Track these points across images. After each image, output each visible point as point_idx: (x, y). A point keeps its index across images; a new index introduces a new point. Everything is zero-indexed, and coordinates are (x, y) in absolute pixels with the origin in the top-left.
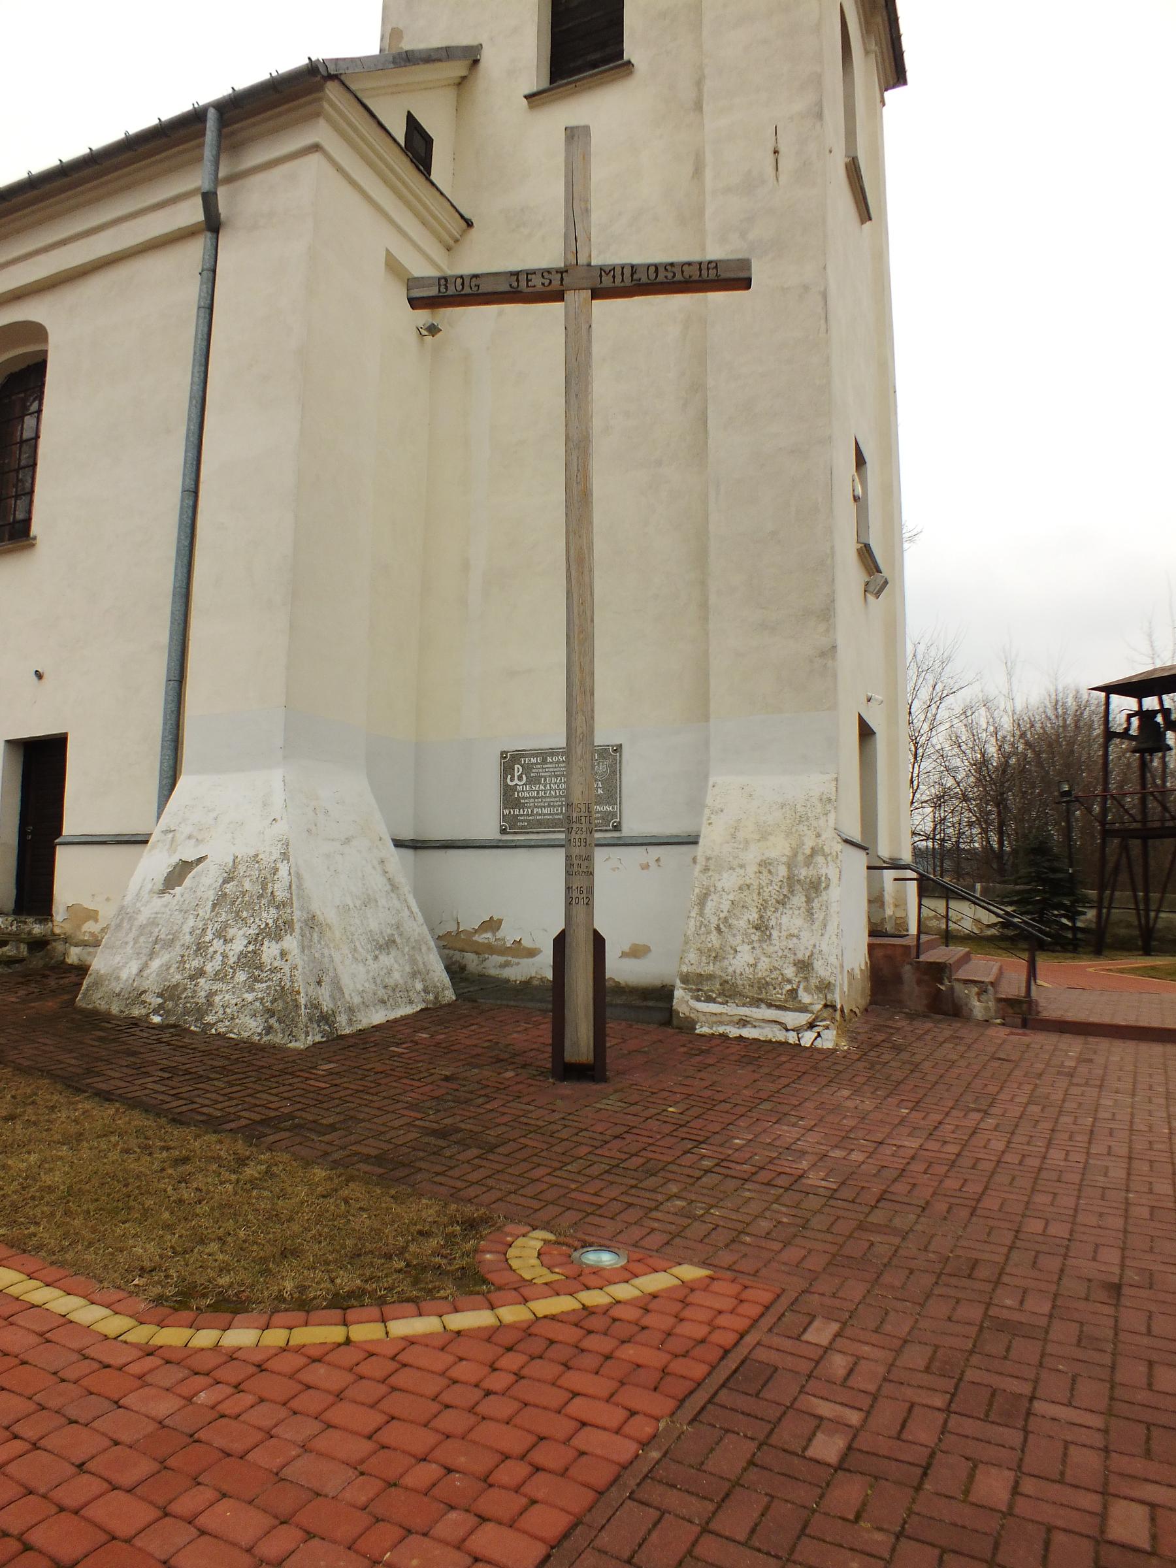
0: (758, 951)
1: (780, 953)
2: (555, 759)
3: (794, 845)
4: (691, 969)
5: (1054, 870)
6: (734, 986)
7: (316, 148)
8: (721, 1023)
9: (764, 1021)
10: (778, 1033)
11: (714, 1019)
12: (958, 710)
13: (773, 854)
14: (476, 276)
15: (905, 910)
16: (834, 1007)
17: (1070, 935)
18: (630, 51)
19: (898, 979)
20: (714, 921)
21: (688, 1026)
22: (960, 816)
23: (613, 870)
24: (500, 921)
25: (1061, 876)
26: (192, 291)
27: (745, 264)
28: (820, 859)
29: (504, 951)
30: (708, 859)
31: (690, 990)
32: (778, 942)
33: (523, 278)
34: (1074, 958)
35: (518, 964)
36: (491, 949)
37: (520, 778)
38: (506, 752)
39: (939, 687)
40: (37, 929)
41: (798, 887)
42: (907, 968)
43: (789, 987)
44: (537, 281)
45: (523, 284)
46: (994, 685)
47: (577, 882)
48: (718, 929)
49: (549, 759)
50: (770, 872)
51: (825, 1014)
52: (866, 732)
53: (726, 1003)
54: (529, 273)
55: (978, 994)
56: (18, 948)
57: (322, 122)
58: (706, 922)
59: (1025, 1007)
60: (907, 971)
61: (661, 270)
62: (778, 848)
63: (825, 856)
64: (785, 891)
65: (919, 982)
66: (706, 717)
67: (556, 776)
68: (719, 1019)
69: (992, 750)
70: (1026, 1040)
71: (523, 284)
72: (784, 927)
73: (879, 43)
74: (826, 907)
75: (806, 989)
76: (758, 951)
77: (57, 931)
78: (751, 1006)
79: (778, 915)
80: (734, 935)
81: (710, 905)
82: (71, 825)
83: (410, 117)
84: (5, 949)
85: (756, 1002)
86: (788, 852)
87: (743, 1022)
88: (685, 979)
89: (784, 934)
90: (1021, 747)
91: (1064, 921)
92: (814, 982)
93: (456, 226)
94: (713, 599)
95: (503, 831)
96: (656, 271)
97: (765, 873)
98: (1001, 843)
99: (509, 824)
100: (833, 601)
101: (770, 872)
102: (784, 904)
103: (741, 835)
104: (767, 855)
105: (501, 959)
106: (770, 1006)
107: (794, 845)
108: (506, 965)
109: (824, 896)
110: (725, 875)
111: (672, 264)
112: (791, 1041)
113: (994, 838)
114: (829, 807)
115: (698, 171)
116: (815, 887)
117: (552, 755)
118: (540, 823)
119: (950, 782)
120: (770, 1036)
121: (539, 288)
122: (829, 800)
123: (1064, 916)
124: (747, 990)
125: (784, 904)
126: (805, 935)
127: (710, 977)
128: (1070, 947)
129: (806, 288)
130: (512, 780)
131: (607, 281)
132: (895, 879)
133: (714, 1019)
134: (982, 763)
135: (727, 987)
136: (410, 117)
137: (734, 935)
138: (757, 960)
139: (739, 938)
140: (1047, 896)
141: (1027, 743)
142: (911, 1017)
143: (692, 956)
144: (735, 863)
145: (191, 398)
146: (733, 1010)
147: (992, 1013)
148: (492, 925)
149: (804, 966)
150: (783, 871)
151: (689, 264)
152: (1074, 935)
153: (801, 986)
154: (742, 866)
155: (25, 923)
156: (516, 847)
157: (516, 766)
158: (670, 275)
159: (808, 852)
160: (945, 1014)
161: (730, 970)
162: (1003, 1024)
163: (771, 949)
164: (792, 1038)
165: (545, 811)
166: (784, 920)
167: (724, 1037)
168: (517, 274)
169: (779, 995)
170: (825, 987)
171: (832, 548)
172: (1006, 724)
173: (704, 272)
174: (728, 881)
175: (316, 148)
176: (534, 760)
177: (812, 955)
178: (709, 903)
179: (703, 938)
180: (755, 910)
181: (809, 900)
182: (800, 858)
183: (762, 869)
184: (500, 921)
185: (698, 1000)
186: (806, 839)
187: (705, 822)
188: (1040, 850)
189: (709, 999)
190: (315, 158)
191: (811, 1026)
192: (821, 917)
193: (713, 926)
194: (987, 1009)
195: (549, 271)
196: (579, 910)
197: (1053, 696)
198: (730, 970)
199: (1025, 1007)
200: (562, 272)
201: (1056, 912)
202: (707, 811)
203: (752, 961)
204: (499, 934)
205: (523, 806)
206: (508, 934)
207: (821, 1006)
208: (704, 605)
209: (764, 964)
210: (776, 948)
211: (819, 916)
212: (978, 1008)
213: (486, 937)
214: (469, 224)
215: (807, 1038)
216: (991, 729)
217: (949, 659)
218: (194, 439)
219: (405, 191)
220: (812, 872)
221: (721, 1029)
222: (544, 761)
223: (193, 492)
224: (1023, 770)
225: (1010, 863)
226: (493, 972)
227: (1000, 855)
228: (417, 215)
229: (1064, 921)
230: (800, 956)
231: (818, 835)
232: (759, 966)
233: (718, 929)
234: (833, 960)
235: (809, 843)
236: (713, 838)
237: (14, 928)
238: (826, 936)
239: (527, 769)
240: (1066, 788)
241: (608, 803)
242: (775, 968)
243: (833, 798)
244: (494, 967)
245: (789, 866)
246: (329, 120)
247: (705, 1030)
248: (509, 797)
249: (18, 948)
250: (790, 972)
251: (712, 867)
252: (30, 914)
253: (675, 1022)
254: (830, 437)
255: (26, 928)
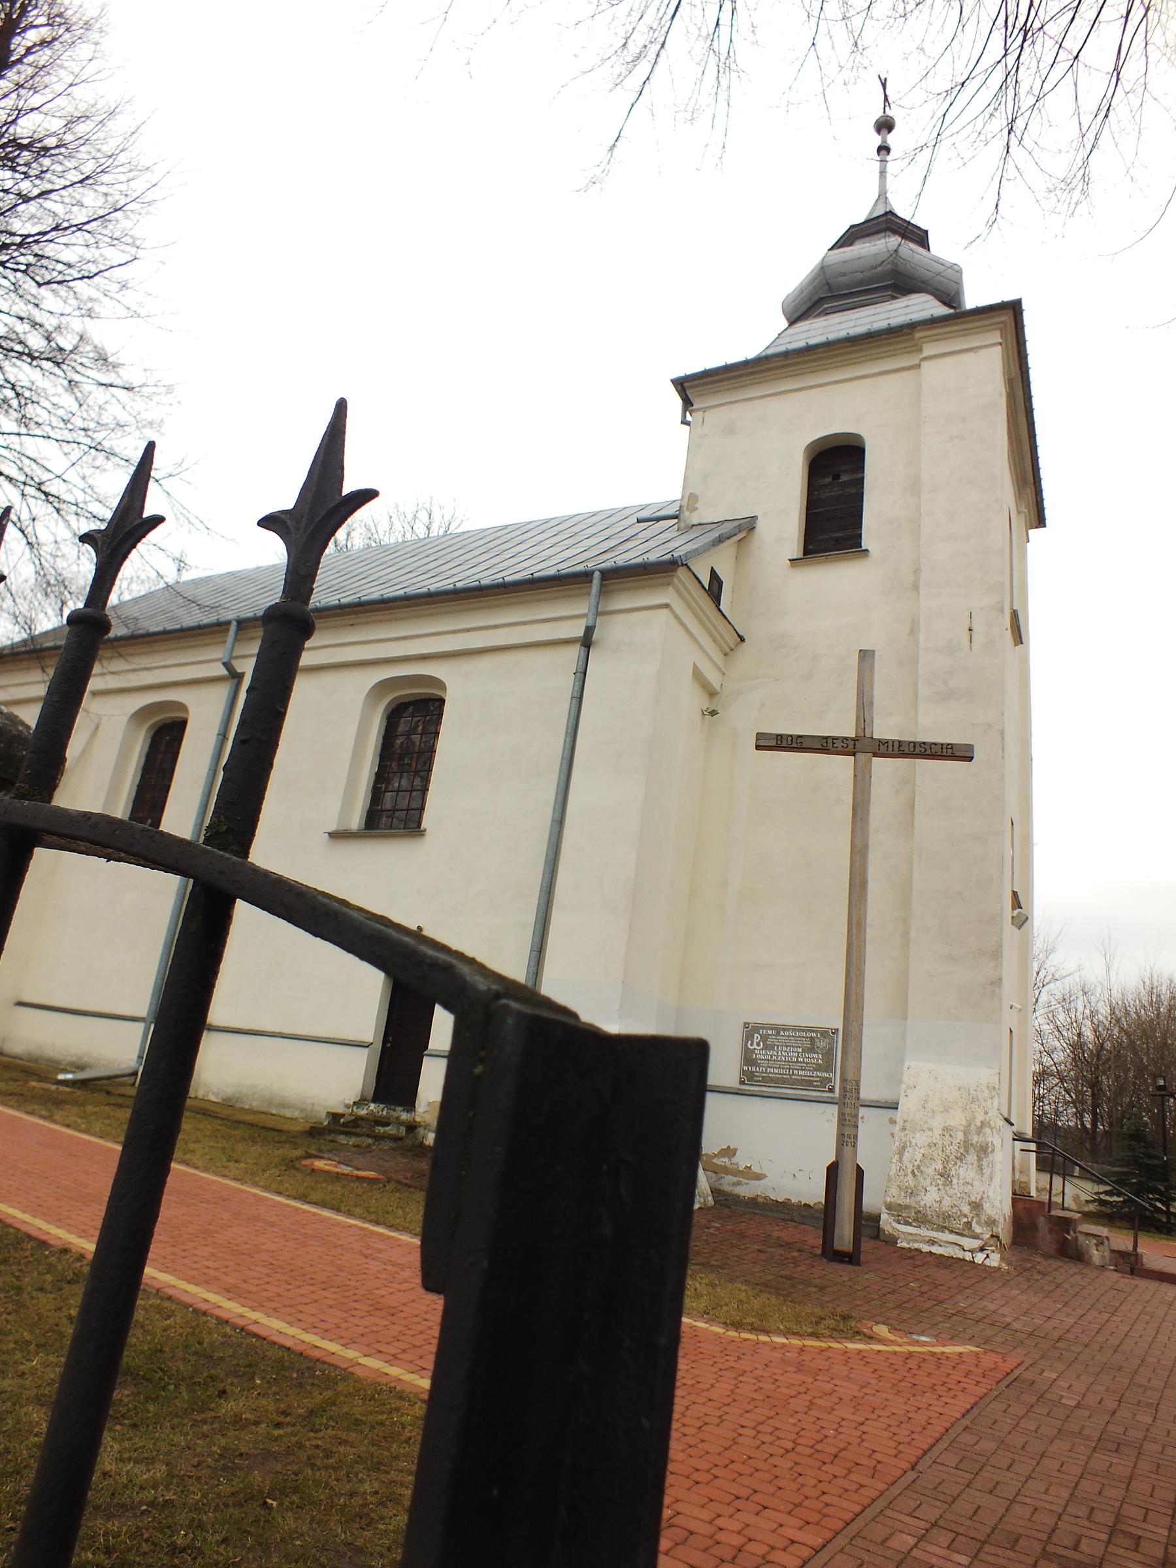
0: (943, 1192)
1: (959, 1195)
2: (787, 1033)
3: (968, 1118)
4: (893, 1200)
5: (1150, 1157)
6: (925, 1215)
7: (667, 606)
8: (917, 1241)
9: (947, 1242)
10: (957, 1251)
11: (911, 1238)
12: (1059, 996)
13: (953, 1123)
14: (800, 736)
15: (1028, 1176)
16: (998, 1237)
17: (1164, 1220)
18: (867, 540)
19: (1034, 1227)
20: (910, 1168)
21: (892, 1241)
22: (1056, 1092)
23: (828, 1121)
24: (735, 1150)
25: (1156, 1162)
26: (567, 683)
27: (970, 748)
28: (987, 1130)
29: (737, 1173)
30: (905, 1121)
31: (893, 1215)
32: (957, 1187)
33: (830, 741)
34: (1167, 1239)
35: (747, 1184)
36: (726, 1171)
37: (758, 1044)
38: (749, 1024)
39: (1041, 975)
40: (404, 1116)
41: (971, 1149)
42: (1042, 1219)
43: (966, 1220)
44: (838, 744)
45: (830, 745)
46: (1094, 972)
47: (847, 1131)
48: (913, 1172)
49: (782, 1033)
50: (951, 1135)
51: (992, 1242)
52: (1011, 1031)
53: (920, 1227)
54: (834, 738)
55: (1097, 1245)
56: (398, 1130)
57: (671, 588)
58: (904, 1167)
59: (1133, 1258)
60: (1041, 1221)
61: (917, 746)
62: (957, 1119)
63: (992, 1129)
64: (962, 1151)
65: (1051, 1231)
66: (906, 1018)
67: (787, 1046)
68: (914, 1238)
69: (1088, 1034)
70: (1133, 1282)
71: (830, 745)
72: (961, 1177)
73: (1028, 507)
74: (992, 1165)
75: (978, 1223)
76: (943, 1192)
77: (418, 1119)
78: (938, 1231)
79: (957, 1167)
80: (925, 1179)
81: (907, 1155)
82: (218, 1013)
83: (712, 570)
84: (387, 1129)
85: (942, 1229)
86: (964, 1123)
87: (932, 1242)
88: (889, 1207)
89: (961, 1181)
90: (1116, 1031)
91: (1159, 1205)
92: (983, 1218)
93: (732, 640)
94: (913, 934)
95: (742, 1083)
96: (914, 747)
97: (947, 1136)
98: (1094, 1123)
99: (748, 1077)
100: (1001, 947)
101: (951, 1135)
102: (961, 1160)
103: (929, 1106)
104: (949, 1122)
105: (735, 1179)
106: (952, 1232)
107: (968, 1118)
108: (738, 1183)
109: (991, 1157)
110: (918, 1135)
111: (924, 743)
112: (967, 1259)
113: (1088, 1118)
114: (994, 1093)
115: (914, 631)
116: (984, 1150)
117: (784, 1030)
118: (772, 1080)
119: (1047, 1061)
120: (952, 1254)
121: (840, 749)
122: (994, 1088)
123: (1160, 1201)
124: (935, 1219)
125: (961, 1160)
126: (977, 1184)
127: (907, 1207)
128: (1164, 1230)
129: (990, 726)
130: (752, 1045)
131: (883, 749)
132: (1022, 1150)
133: (911, 1238)
134: (1078, 1046)
135: (920, 1215)
136: (712, 570)
137: (925, 1179)
138: (942, 1198)
139: (928, 1182)
140: (1143, 1180)
141: (1122, 1029)
142: (1046, 1256)
143: (894, 1191)
144: (925, 1127)
145: (563, 758)
146: (923, 1232)
147: (1107, 1261)
148: (729, 1152)
149: (976, 1206)
150: (960, 1136)
151: (935, 744)
152: (1168, 1219)
153: (974, 1220)
154: (930, 1129)
155: (395, 1110)
156: (752, 1095)
157: (756, 1035)
158: (923, 750)
159: (979, 1124)
160: (1071, 1258)
161: (922, 1203)
162: (1116, 1270)
163: (951, 1192)
164: (968, 1256)
165: (776, 1071)
166: (962, 1171)
167: (918, 1250)
168: (826, 738)
169: (958, 1225)
170: (991, 1222)
171: (1002, 909)
172: (1104, 1011)
173: (945, 750)
174: (921, 1139)
175: (667, 606)
176: (770, 1032)
177: (982, 1198)
178: (906, 1154)
179: (902, 1178)
180: (940, 1162)
181: (979, 1159)
182: (973, 1128)
183: (945, 1133)
184: (735, 1150)
185: (899, 1223)
186: (977, 1115)
187: (903, 1094)
188: (1137, 1136)
189: (907, 1223)
190: (665, 611)
191: (982, 1249)
192: (988, 1173)
193: (910, 1170)
194: (1103, 1257)
195: (846, 739)
196: (848, 1150)
197: (1148, 983)
198: (922, 1203)
199: (1133, 1258)
200: (852, 739)
201: (1151, 1196)
202: (904, 1086)
203: (938, 1199)
204: (734, 1160)
205: (759, 1065)
206: (742, 1161)
207: (988, 1236)
208: (906, 935)
209: (947, 1202)
210: (956, 1191)
211: (987, 1171)
212: (1096, 1255)
213: (723, 1161)
214: (742, 639)
215: (980, 1258)
216: (1087, 1012)
217: (1053, 950)
218: (563, 786)
219: (712, 628)
220: (981, 1139)
221: (916, 1245)
222: (778, 1034)
223: (559, 822)
224: (1118, 1056)
225: (1103, 1145)
226: (727, 1188)
227: (1092, 1134)
228: (711, 635)
229: (1159, 1205)
230: (973, 1199)
231: (986, 1113)
232: (944, 1202)
233: (913, 1172)
234: (997, 1204)
235: (980, 1118)
236: (909, 1106)
237: (385, 1113)
238: (992, 1186)
239: (764, 1038)
240: (1161, 1082)
241: (827, 1072)
242: (955, 1206)
243: (997, 1087)
244: (729, 1184)
245: (966, 1133)
246: (678, 592)
247: (905, 1245)
248: (748, 1059)
249: (398, 1130)
250: (966, 1209)
251: (908, 1127)
252: (400, 1105)
253: (882, 1237)
254: (1003, 832)
255: (395, 1114)
